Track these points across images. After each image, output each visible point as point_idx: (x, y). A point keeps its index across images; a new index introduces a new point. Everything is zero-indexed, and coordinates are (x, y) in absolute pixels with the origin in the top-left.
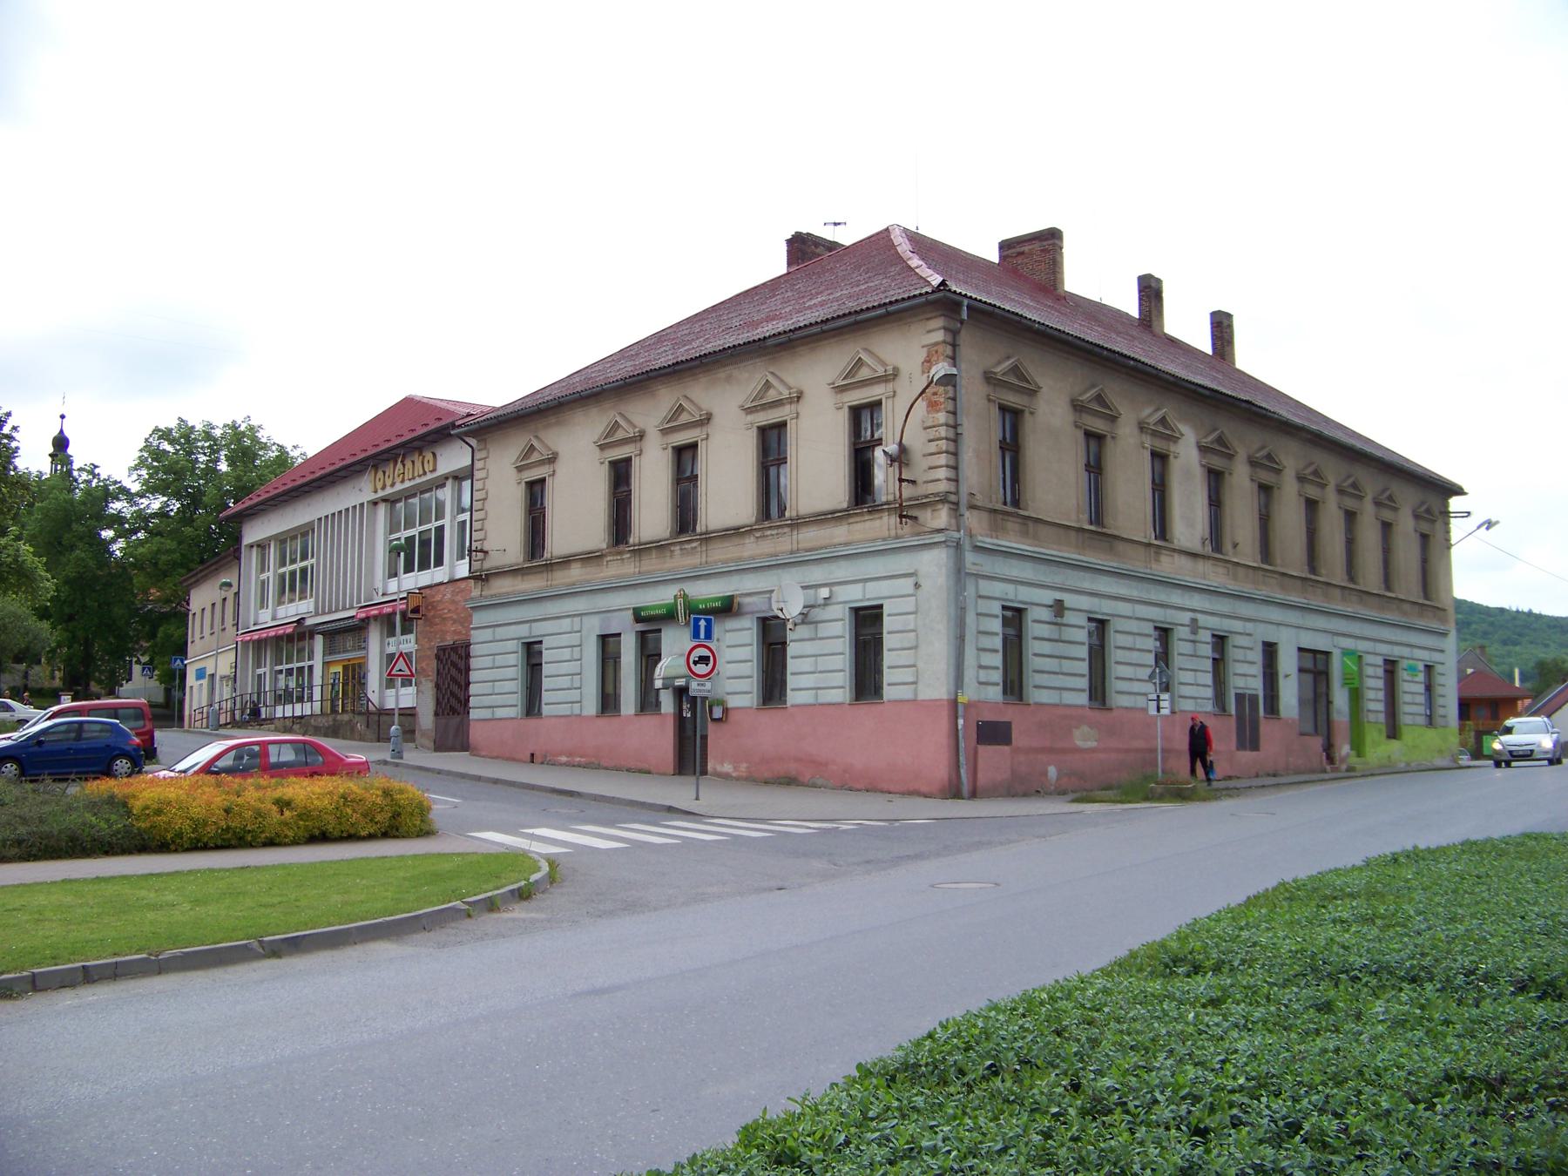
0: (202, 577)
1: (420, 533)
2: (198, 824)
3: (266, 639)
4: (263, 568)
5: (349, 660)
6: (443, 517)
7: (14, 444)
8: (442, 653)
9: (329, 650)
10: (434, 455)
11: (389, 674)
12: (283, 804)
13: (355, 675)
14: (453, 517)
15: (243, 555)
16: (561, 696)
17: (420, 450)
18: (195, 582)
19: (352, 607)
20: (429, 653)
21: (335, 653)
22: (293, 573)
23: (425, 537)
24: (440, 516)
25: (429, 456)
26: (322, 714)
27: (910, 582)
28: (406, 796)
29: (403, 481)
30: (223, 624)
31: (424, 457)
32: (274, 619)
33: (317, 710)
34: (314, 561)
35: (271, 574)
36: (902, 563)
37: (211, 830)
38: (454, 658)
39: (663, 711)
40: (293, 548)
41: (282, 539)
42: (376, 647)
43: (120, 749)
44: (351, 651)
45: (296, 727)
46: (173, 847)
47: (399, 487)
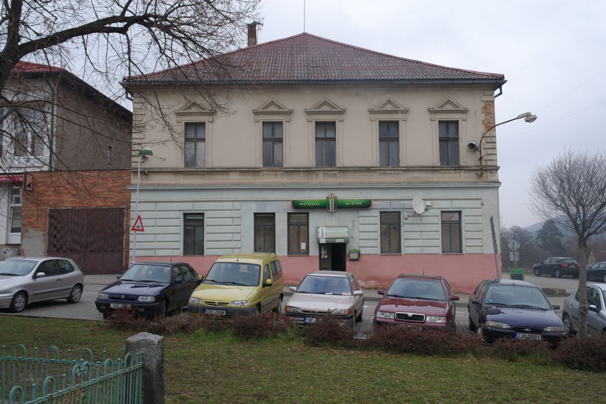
16: (413, 243)
27: (480, 202)
36: (473, 194)
39: (310, 254)
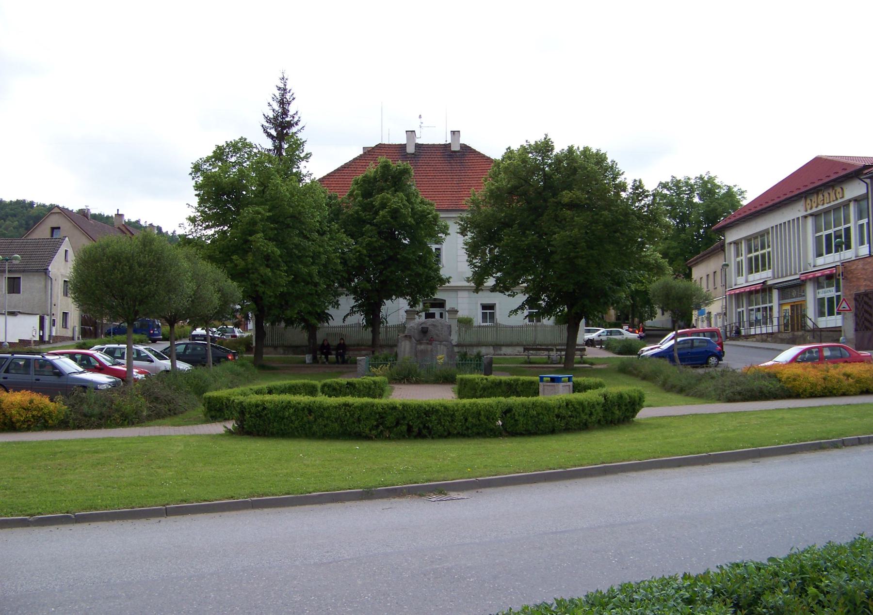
0: (700, 261)
1: (835, 232)
2: (814, 385)
3: (742, 292)
4: (738, 254)
5: (794, 302)
6: (849, 222)
7: (233, 142)
8: (858, 297)
9: (782, 297)
10: (842, 189)
11: (838, 310)
12: (848, 376)
13: (798, 311)
14: (855, 223)
15: (726, 249)
17: (833, 187)
18: (695, 264)
19: (795, 274)
20: (850, 297)
21: (785, 299)
22: (757, 257)
23: (838, 234)
24: (847, 221)
25: (839, 190)
26: (779, 332)
28: (797, 382)
29: (823, 204)
30: (714, 286)
31: (836, 190)
32: (747, 281)
33: (775, 329)
34: (770, 249)
35: (743, 258)
37: (819, 388)
38: (866, 299)
40: (756, 243)
41: (748, 239)
42: (811, 297)
43: (712, 352)
44: (796, 297)
45: (769, 339)
46: (802, 396)
47: (820, 208)
